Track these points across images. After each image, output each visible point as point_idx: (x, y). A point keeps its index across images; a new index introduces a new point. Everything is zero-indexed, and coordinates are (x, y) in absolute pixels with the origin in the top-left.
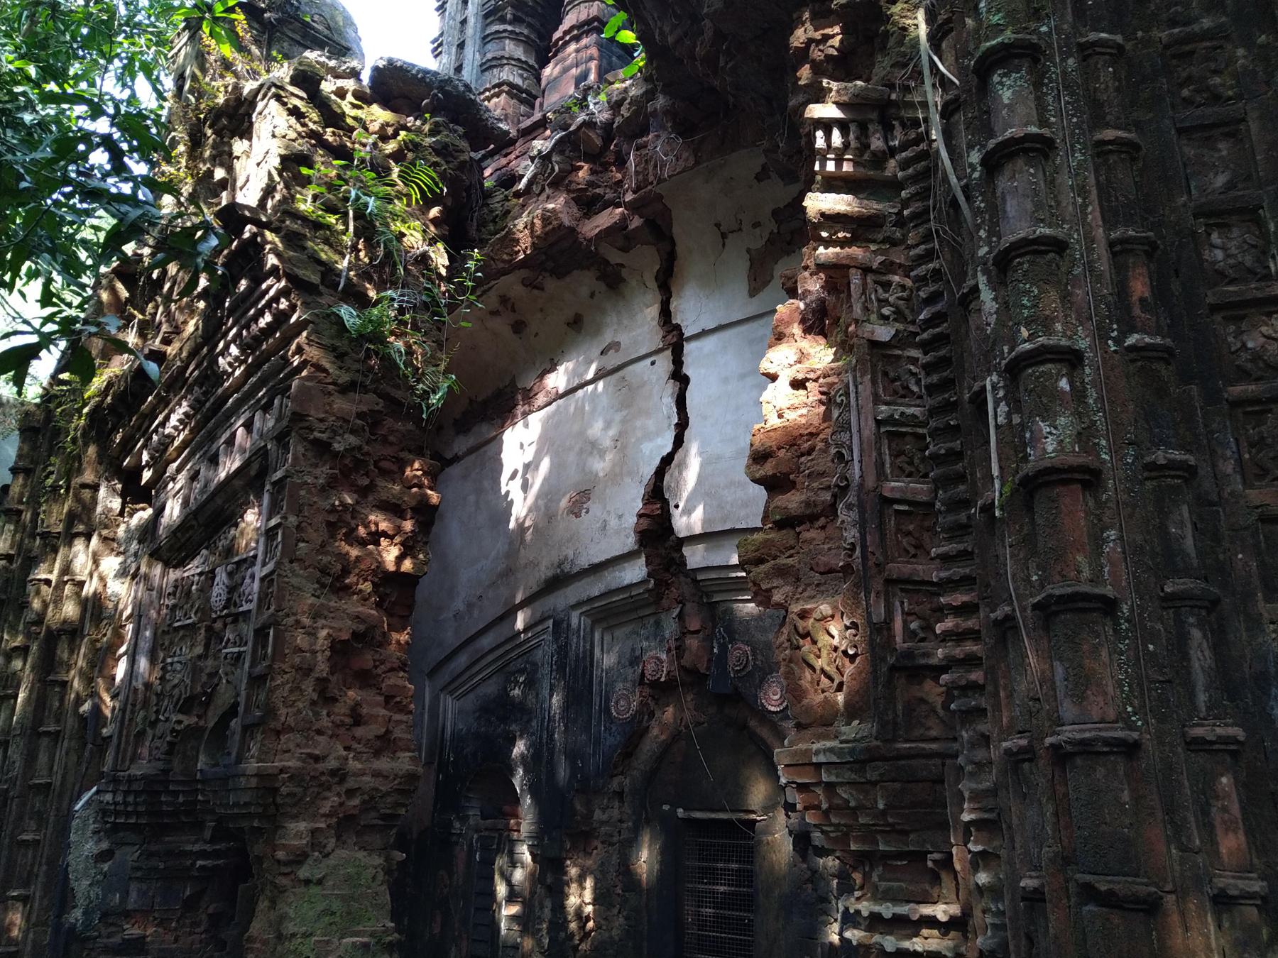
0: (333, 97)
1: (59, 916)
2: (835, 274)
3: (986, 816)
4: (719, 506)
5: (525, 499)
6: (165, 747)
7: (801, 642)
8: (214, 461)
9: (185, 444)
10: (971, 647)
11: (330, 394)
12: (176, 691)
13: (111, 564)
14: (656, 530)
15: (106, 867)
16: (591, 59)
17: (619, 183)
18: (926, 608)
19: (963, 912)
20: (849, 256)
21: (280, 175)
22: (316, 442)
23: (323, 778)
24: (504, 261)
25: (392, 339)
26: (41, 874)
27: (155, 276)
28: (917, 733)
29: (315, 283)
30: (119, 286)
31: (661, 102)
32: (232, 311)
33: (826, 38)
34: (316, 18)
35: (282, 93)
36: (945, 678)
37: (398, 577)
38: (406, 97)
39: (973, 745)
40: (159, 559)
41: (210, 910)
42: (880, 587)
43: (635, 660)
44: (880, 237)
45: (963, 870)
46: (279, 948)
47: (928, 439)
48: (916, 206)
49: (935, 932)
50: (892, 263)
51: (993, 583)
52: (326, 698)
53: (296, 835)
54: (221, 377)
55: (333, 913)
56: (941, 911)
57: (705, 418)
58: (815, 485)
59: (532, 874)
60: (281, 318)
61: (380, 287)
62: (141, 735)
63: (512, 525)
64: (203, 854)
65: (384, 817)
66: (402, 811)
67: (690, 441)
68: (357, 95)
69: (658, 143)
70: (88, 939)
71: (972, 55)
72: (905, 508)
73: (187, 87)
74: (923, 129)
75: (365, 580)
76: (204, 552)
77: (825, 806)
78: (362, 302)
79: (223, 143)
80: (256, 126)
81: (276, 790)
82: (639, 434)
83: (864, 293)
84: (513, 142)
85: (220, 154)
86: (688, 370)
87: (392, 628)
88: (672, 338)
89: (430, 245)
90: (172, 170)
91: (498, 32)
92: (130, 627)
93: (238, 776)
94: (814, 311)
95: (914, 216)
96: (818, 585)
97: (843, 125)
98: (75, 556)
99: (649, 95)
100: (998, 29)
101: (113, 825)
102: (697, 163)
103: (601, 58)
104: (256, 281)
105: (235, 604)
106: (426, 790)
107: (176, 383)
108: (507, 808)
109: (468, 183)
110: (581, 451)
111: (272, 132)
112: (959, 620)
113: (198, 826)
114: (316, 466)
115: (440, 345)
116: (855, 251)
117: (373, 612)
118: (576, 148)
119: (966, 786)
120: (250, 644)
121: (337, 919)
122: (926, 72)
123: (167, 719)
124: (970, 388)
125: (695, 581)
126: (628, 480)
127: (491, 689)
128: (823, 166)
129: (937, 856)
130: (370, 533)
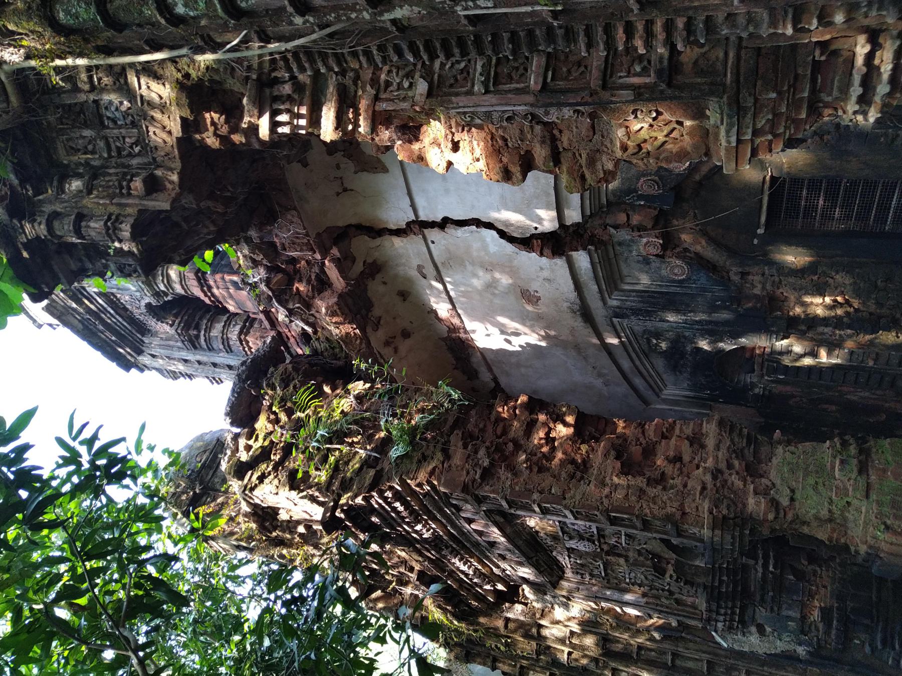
0: (251, 453)
2: (378, 120)
3: (790, 16)
5: (525, 334)
6: (688, 587)
7: (644, 150)
8: (493, 544)
9: (480, 561)
12: (650, 577)
13: (559, 613)
14: (553, 243)
15: (768, 629)
16: (223, 278)
19: (865, 32)
20: (366, 111)
21: (302, 491)
22: (483, 477)
23: (718, 485)
24: (361, 343)
25: (413, 422)
26: (770, 670)
27: (367, 573)
29: (375, 473)
30: (374, 596)
31: (253, 233)
32: (392, 528)
33: (213, 123)
34: (198, 459)
35: (249, 486)
36: (680, 47)
39: (734, 26)
40: (558, 583)
41: (806, 563)
43: (646, 261)
44: (353, 88)
46: (838, 521)
47: (501, 56)
48: (332, 62)
49: (878, 54)
50: (372, 79)
52: (661, 480)
53: (757, 505)
54: (436, 537)
55: (816, 483)
56: (862, 49)
57: (473, 207)
58: (529, 136)
60: (398, 496)
61: (378, 429)
62: (678, 602)
63: (543, 344)
64: (765, 566)
65: (749, 443)
66: (745, 431)
67: (489, 217)
68: (249, 438)
69: (282, 235)
72: (550, 74)
73: (244, 544)
74: (277, 56)
75: (579, 448)
76: (554, 553)
77: (770, 137)
78: (387, 442)
79: (281, 526)
80: (270, 504)
81: (724, 517)
83: (392, 100)
84: (279, 334)
85: (289, 528)
86: (439, 218)
87: (614, 432)
88: (416, 228)
89: (349, 393)
90: (299, 558)
91: (205, 340)
92: (603, 604)
93: (712, 542)
94: (403, 134)
95: (339, 64)
96: (603, 137)
97: (274, 113)
98: (553, 635)
99: (248, 241)
101: (741, 623)
102: (295, 209)
103: (224, 272)
104: (373, 511)
106: (729, 411)
107: (439, 564)
108: (748, 355)
109: (307, 366)
110: (494, 294)
111: (273, 494)
113: (745, 568)
114: (499, 478)
115: (417, 390)
116: (363, 104)
117: (602, 444)
118: (284, 292)
120: (620, 529)
121: (820, 481)
122: (238, 55)
123: (669, 584)
124: (466, 26)
125: (591, 216)
126: (515, 263)
127: (660, 363)
128: (302, 128)
129: (817, 53)
130: (547, 444)
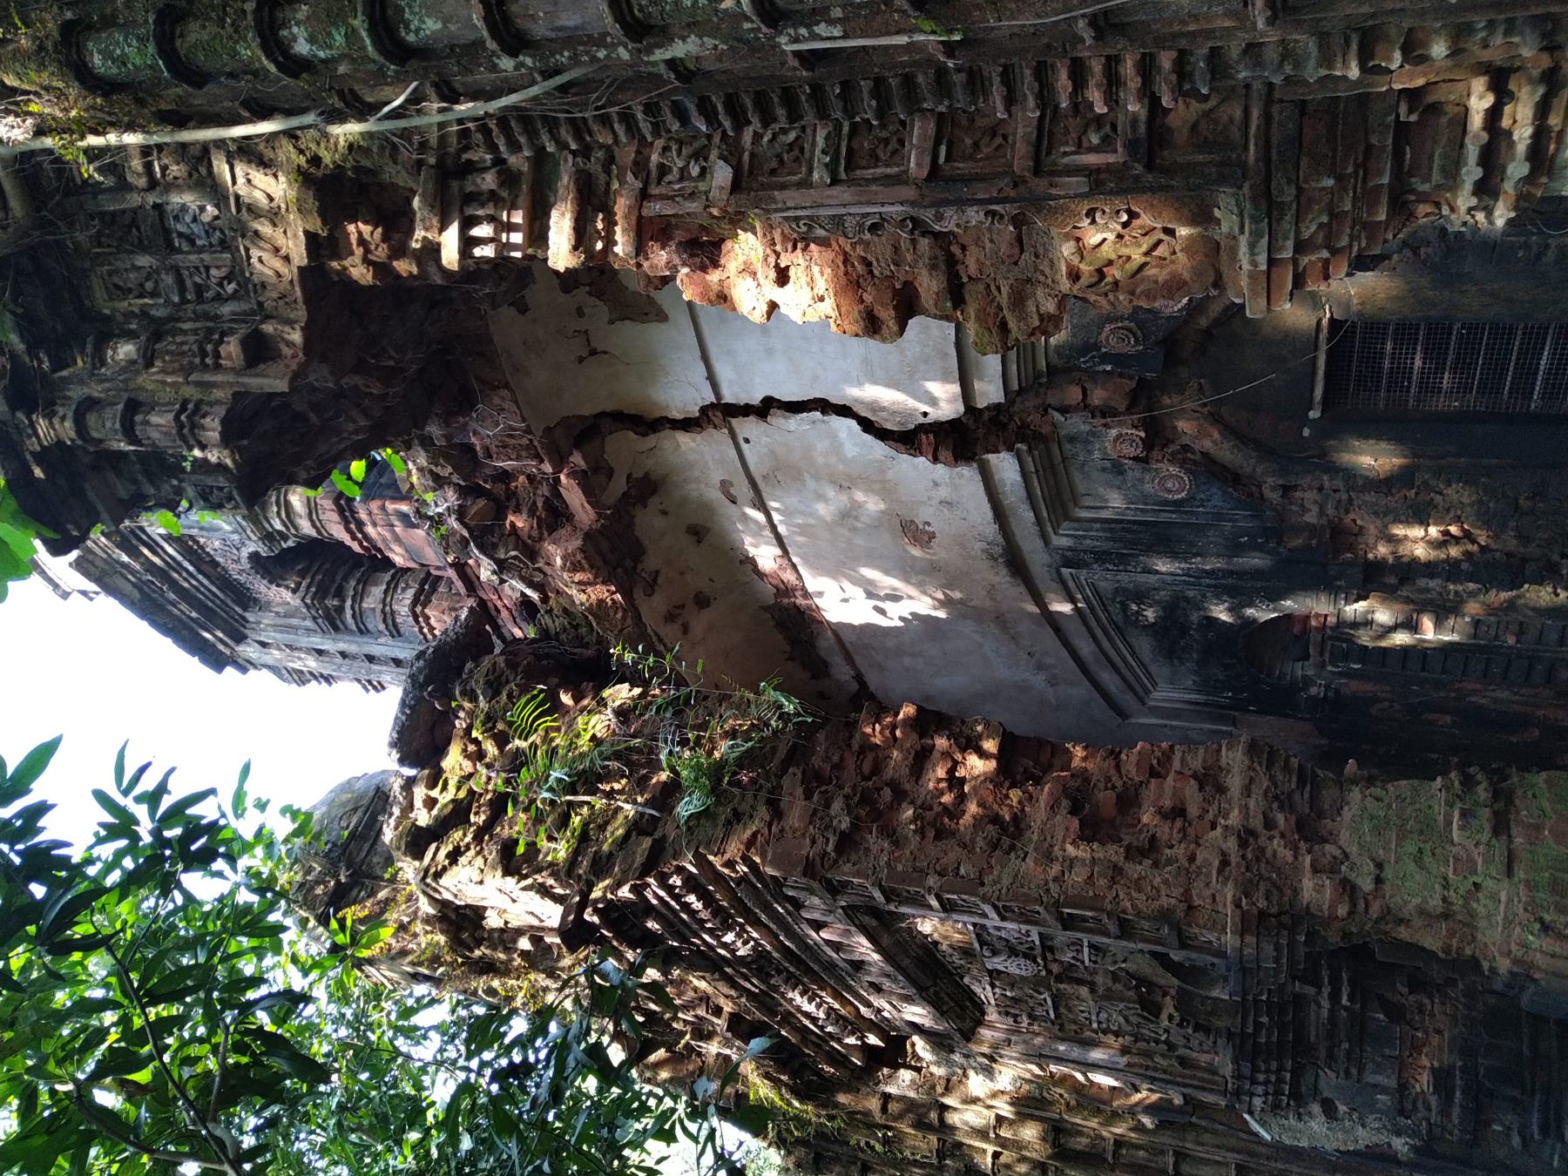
0: (435, 812)
1: (1399, 1163)
2: (647, 232)
3: (1354, 47)
4: (926, 362)
5: (910, 597)
7: (1109, 279)
8: (859, 966)
9: (837, 996)
10: (1128, 68)
11: (782, 831)
12: (1134, 1019)
13: (977, 1084)
14: (954, 440)
15: (1342, 1108)
16: (383, 508)
17: (531, 478)
18: (1074, 124)
21: (526, 877)
22: (839, 849)
23: (1249, 856)
24: (624, 618)
25: (717, 755)
27: (641, 1019)
28: (1235, 134)
29: (652, 844)
30: (652, 1058)
31: (434, 430)
32: (684, 939)
33: (362, 241)
34: (344, 824)
35: (433, 870)
36: (1166, 101)
37: (1004, 758)
38: (432, 729)
39: (1258, 64)
42: (1043, 182)
43: (1117, 468)
44: (602, 178)
45: (1425, 75)
47: (858, 119)
49: (1507, 109)
50: (636, 163)
51: (1046, 40)
52: (1149, 849)
53: (1318, 892)
54: (759, 955)
55: (1420, 851)
56: (1480, 103)
57: (815, 378)
58: (909, 258)
59: (1383, 601)
60: (692, 884)
61: (656, 767)
62: (1183, 1062)
63: (942, 614)
64: (1335, 997)
65: (1302, 782)
66: (1295, 762)
67: (844, 396)
68: (432, 786)
69: (483, 433)
70: (1430, 1132)
71: (383, 66)
73: (426, 972)
74: (470, 125)
75: (1007, 796)
76: (966, 980)
77: (1325, 254)
78: (672, 790)
79: (490, 939)
80: (470, 902)
81: (1261, 913)
82: (833, 460)
83: (671, 198)
84: (482, 603)
86: (756, 399)
88: (717, 417)
89: (605, 705)
90: (521, 994)
91: (354, 616)
92: (1053, 1068)
94: (692, 256)
95: (578, 136)
96: (1037, 256)
97: (468, 223)
98: (966, 1123)
99: (427, 443)
100: (352, 35)
102: (507, 386)
103: (383, 497)
104: (649, 911)
105: (1032, 949)
106: (1268, 727)
107: (766, 1001)
108: (1296, 629)
110: (854, 529)
112: (1092, 83)
114: (867, 850)
115: (723, 698)
116: (621, 206)
118: (489, 530)
119: (1313, 72)
120: (1080, 935)
121: (1428, 846)
122: (402, 123)
123: (1167, 1031)
124: (795, 69)
126: (890, 475)
127: (1144, 645)
128: (515, 247)
129: (1403, 109)
